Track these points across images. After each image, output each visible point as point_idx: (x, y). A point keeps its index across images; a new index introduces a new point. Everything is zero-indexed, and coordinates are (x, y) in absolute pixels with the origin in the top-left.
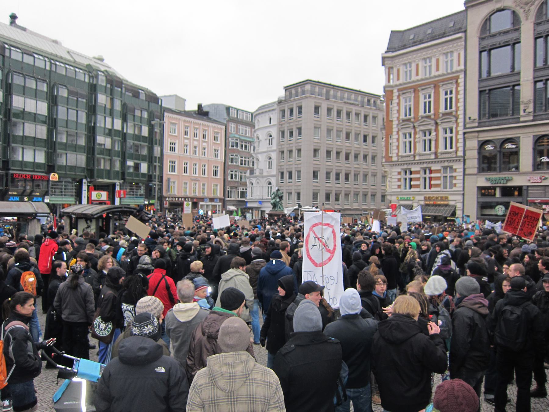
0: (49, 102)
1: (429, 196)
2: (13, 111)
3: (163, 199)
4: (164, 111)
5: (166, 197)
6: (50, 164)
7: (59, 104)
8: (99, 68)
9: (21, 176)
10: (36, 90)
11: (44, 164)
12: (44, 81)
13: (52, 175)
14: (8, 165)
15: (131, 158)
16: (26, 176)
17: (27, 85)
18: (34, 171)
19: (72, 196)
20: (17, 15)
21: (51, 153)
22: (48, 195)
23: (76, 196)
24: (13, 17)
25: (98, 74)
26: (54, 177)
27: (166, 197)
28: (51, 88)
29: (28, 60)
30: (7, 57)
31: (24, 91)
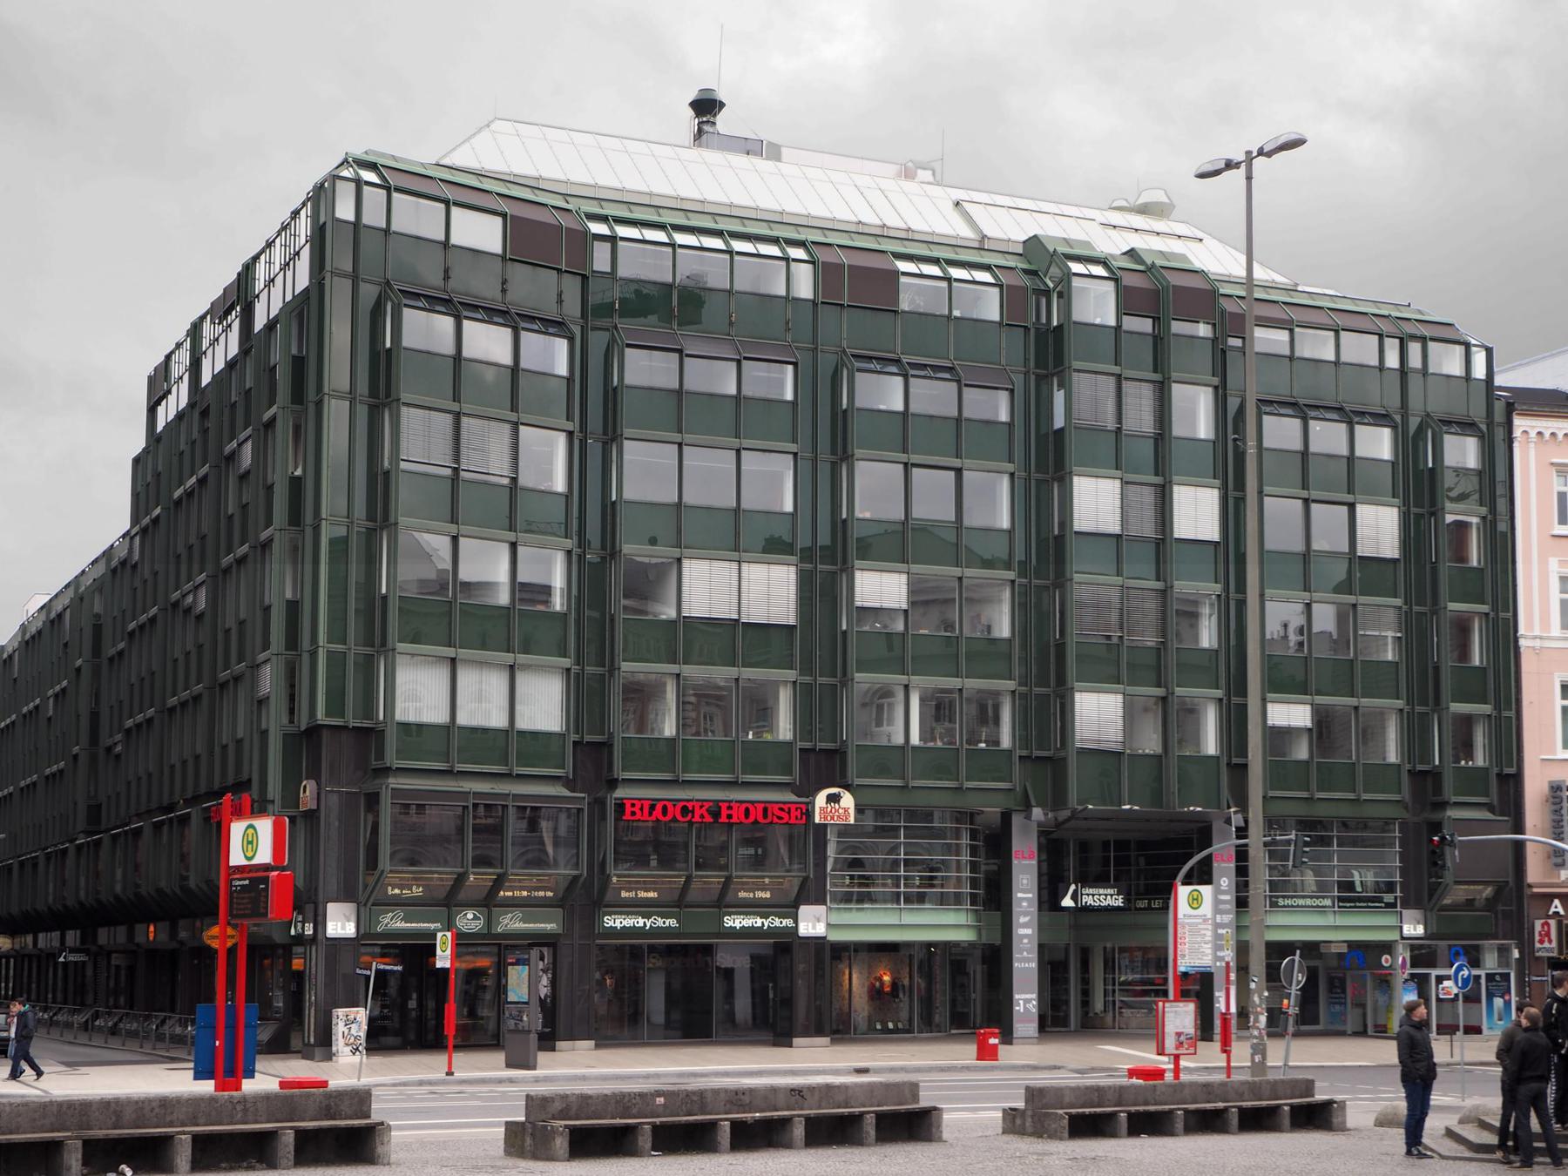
0: (1406, 503)
1: (1555, 585)
2: (856, 532)
3: (1530, 908)
4: (1510, 409)
5: (1550, 898)
6: (1420, 767)
7: (858, 452)
8: (1184, 257)
9: (665, 809)
10: (1305, 454)
11: (561, 736)
12: (1381, 419)
13: (821, 799)
14: (1438, 789)
15: (1109, 668)
16: (685, 810)
17: (1360, 452)
18: (674, 783)
19: (958, 899)
20: (721, 96)
21: (1044, 700)
22: (820, 901)
23: (974, 899)
24: (706, 106)
25: (1069, 275)
26: (835, 807)
27: (1550, 898)
28: (1409, 445)
29: (1318, 346)
30: (1415, 371)
31: (679, 414)
